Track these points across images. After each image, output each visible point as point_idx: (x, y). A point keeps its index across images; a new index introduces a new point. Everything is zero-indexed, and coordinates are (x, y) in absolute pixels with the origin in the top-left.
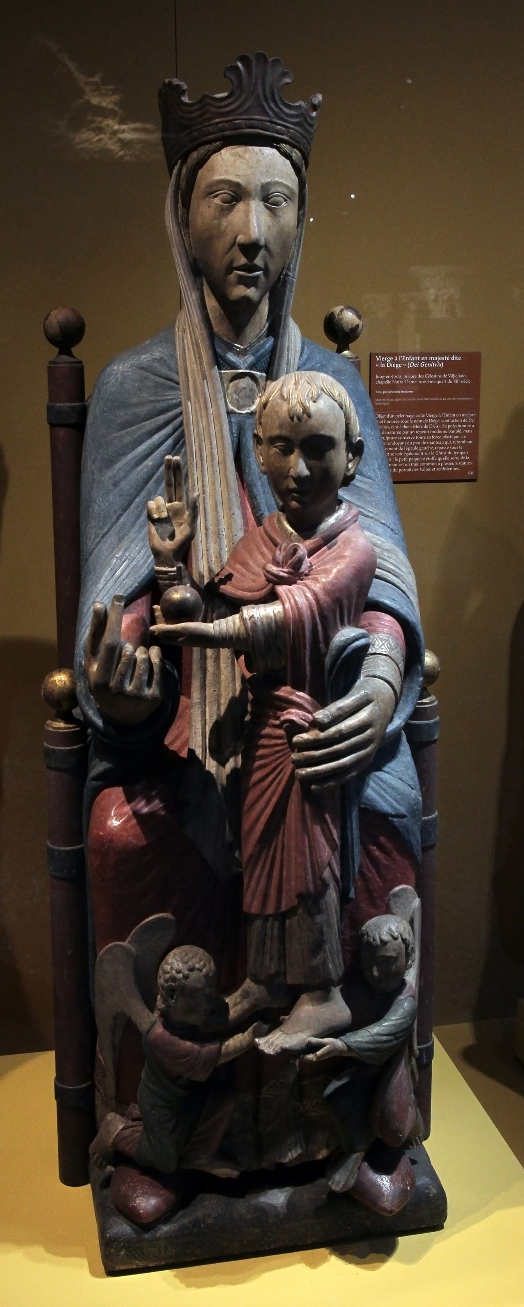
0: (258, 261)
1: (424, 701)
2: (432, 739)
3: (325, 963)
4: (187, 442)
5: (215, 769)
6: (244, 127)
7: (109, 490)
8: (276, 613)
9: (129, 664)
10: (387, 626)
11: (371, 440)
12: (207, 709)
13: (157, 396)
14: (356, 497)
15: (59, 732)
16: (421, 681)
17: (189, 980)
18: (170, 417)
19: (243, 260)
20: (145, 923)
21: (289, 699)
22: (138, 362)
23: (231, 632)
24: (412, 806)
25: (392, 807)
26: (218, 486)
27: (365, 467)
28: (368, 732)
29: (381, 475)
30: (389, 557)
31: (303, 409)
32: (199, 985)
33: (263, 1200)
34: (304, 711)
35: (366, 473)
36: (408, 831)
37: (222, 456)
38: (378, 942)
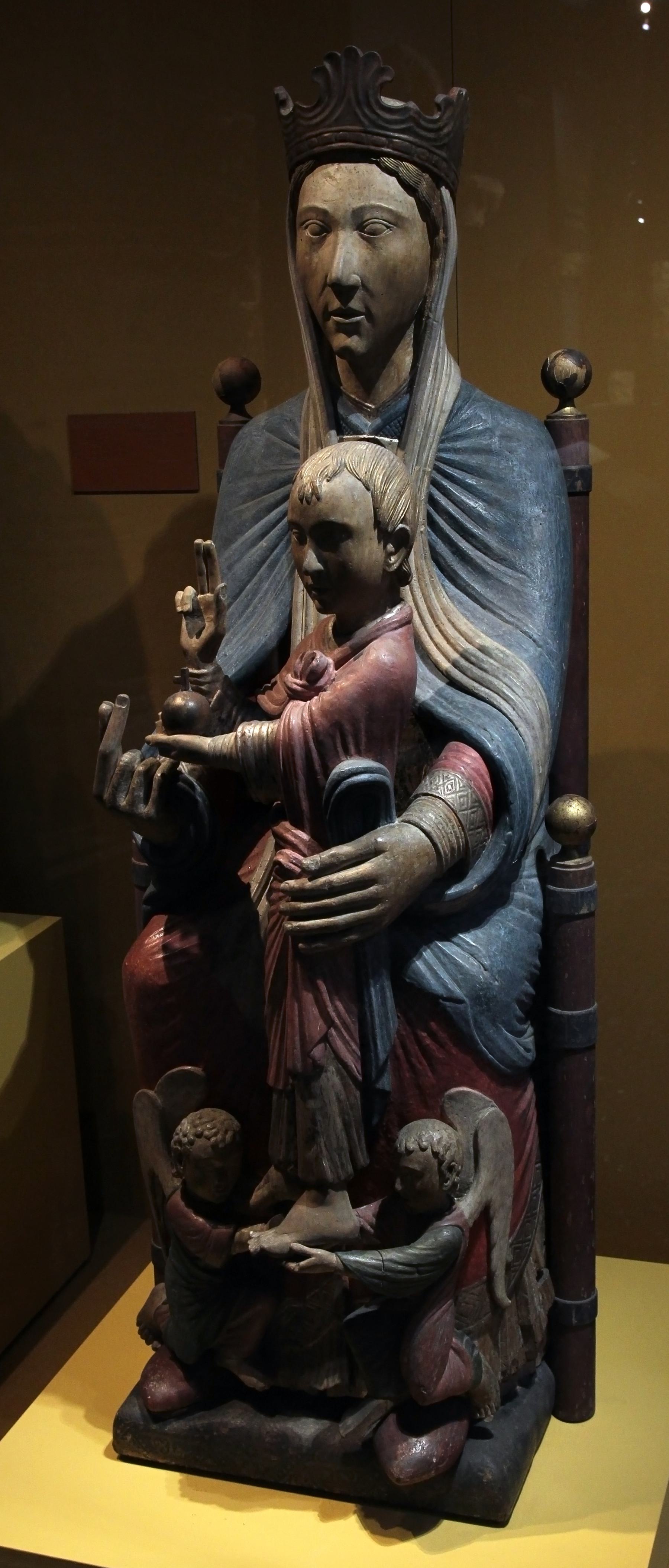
0: (355, 304)
1: (567, 863)
2: (576, 914)
3: (318, 1159)
14: (501, 596)
17: (194, 1146)
19: (336, 304)
27: (520, 559)
28: (372, 889)
29: (541, 570)
31: (312, 489)
32: (203, 1156)
33: (290, 1426)
35: (521, 566)
38: (403, 1149)
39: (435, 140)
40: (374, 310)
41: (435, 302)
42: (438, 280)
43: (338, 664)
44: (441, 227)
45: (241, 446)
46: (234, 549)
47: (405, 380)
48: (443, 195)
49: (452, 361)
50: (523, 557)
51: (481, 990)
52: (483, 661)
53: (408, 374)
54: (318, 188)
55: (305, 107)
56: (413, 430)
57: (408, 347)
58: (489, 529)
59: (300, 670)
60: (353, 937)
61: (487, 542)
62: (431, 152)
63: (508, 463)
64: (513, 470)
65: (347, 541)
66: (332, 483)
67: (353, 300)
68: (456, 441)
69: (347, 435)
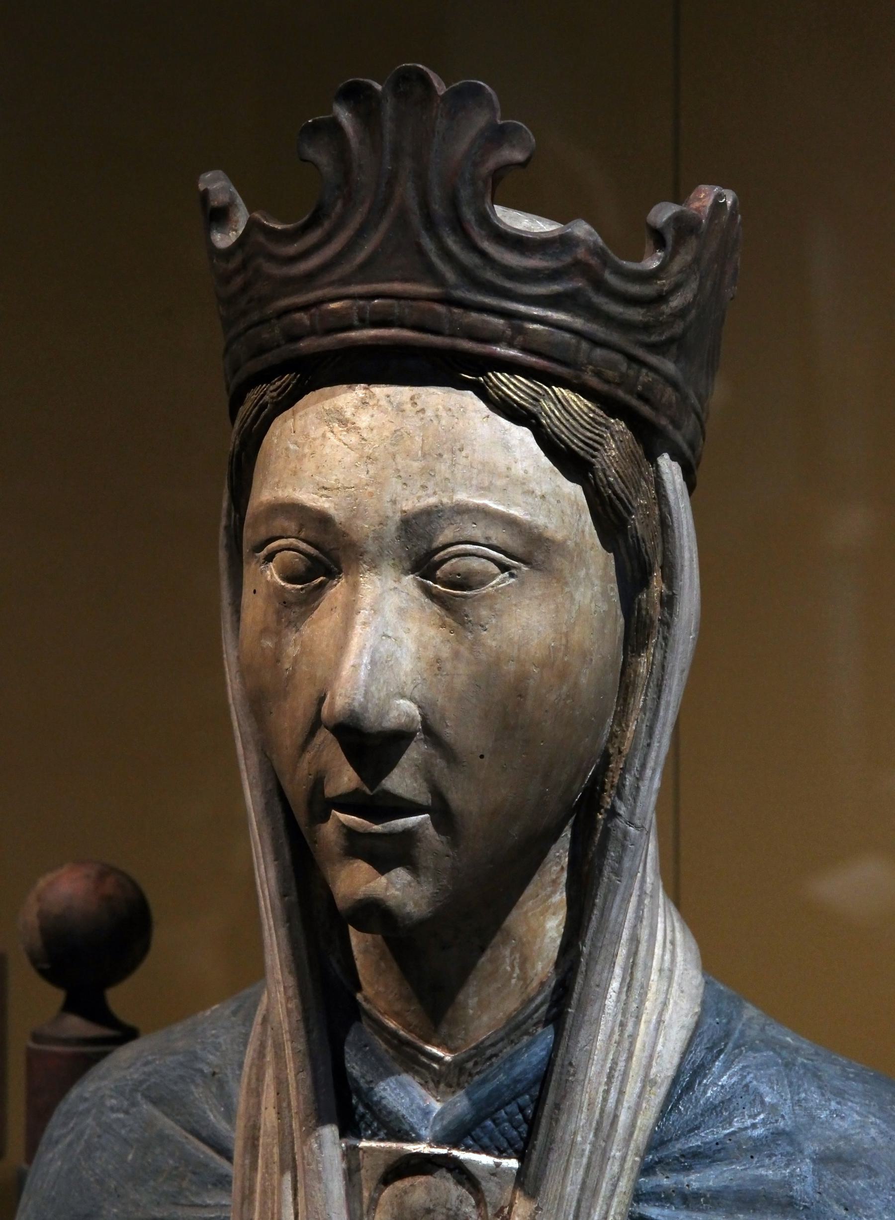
6: (356, 323)
39: (646, 328)
40: (456, 798)
41: (634, 771)
42: (644, 709)
44: (657, 567)
47: (542, 984)
48: (665, 477)
49: (677, 925)
53: (550, 968)
54: (306, 450)
55: (279, 227)
56: (562, 1140)
57: (554, 892)
62: (632, 359)
67: (396, 771)
68: (688, 1169)
69: (370, 1138)
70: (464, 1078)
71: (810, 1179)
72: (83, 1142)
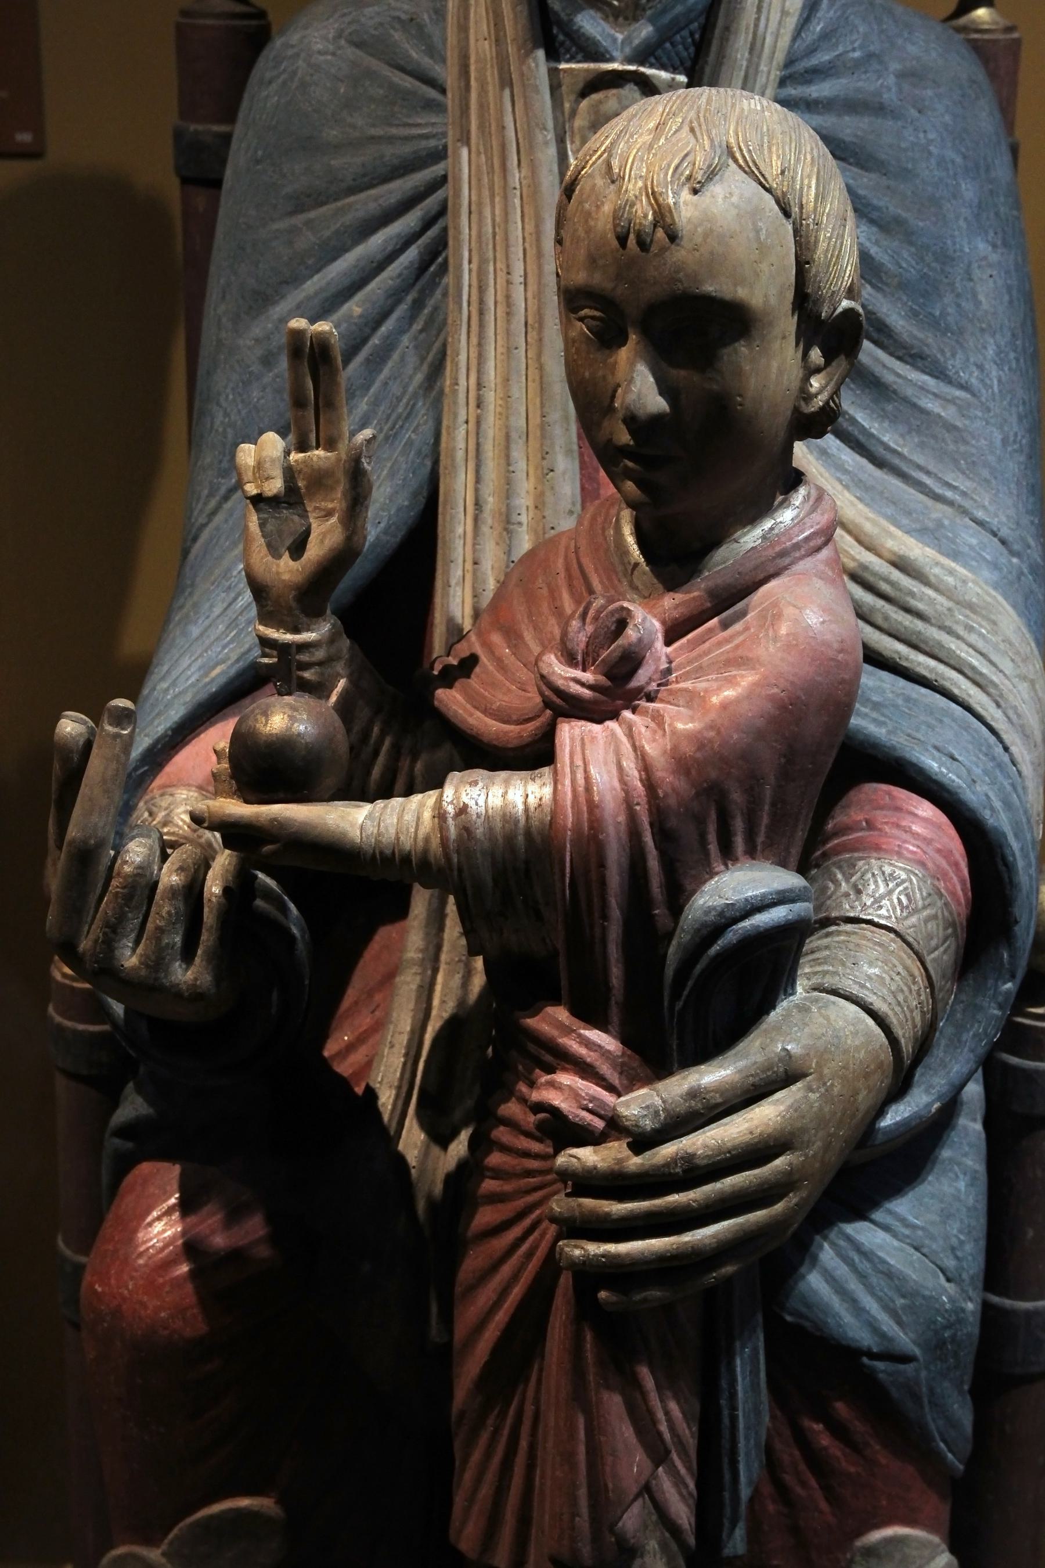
4: (451, 261)
5: (416, 1152)
7: (251, 373)
8: (532, 809)
9: (128, 898)
10: (916, 835)
11: (985, 277)
12: (440, 978)
13: (391, 125)
14: (916, 440)
15: (73, 988)
16: (1008, 992)
18: (416, 187)
20: (203, 1517)
21: (558, 1045)
22: (353, 27)
23: (407, 843)
24: (936, 1332)
25: (874, 1328)
26: (517, 391)
27: (954, 355)
28: (780, 1163)
29: (1000, 381)
30: (970, 629)
31: (654, 213)
34: (597, 1085)
35: (957, 372)
36: (916, 1398)
37: (536, 307)
43: (673, 633)
45: (283, 77)
46: (275, 317)
50: (959, 351)
51: (946, 1327)
52: (912, 594)
58: (885, 288)
59: (582, 646)
60: (729, 1269)
61: (883, 316)
63: (917, 137)
64: (930, 153)
65: (736, 344)
66: (704, 200)
68: (809, 82)
69: (568, 61)
70: (638, 12)
71: (894, 90)
72: (296, 79)
